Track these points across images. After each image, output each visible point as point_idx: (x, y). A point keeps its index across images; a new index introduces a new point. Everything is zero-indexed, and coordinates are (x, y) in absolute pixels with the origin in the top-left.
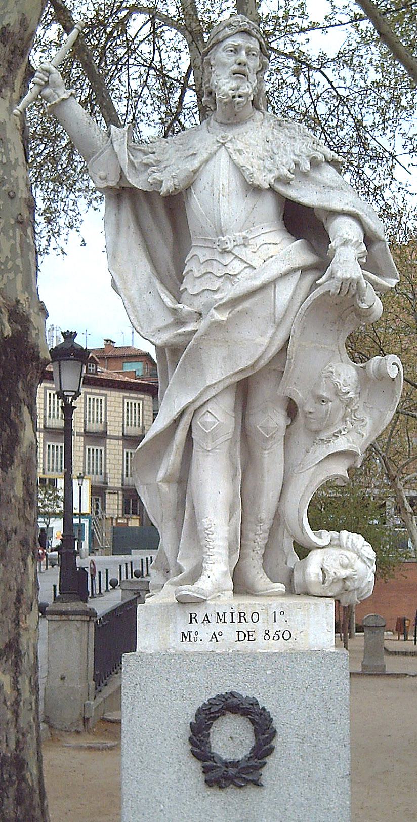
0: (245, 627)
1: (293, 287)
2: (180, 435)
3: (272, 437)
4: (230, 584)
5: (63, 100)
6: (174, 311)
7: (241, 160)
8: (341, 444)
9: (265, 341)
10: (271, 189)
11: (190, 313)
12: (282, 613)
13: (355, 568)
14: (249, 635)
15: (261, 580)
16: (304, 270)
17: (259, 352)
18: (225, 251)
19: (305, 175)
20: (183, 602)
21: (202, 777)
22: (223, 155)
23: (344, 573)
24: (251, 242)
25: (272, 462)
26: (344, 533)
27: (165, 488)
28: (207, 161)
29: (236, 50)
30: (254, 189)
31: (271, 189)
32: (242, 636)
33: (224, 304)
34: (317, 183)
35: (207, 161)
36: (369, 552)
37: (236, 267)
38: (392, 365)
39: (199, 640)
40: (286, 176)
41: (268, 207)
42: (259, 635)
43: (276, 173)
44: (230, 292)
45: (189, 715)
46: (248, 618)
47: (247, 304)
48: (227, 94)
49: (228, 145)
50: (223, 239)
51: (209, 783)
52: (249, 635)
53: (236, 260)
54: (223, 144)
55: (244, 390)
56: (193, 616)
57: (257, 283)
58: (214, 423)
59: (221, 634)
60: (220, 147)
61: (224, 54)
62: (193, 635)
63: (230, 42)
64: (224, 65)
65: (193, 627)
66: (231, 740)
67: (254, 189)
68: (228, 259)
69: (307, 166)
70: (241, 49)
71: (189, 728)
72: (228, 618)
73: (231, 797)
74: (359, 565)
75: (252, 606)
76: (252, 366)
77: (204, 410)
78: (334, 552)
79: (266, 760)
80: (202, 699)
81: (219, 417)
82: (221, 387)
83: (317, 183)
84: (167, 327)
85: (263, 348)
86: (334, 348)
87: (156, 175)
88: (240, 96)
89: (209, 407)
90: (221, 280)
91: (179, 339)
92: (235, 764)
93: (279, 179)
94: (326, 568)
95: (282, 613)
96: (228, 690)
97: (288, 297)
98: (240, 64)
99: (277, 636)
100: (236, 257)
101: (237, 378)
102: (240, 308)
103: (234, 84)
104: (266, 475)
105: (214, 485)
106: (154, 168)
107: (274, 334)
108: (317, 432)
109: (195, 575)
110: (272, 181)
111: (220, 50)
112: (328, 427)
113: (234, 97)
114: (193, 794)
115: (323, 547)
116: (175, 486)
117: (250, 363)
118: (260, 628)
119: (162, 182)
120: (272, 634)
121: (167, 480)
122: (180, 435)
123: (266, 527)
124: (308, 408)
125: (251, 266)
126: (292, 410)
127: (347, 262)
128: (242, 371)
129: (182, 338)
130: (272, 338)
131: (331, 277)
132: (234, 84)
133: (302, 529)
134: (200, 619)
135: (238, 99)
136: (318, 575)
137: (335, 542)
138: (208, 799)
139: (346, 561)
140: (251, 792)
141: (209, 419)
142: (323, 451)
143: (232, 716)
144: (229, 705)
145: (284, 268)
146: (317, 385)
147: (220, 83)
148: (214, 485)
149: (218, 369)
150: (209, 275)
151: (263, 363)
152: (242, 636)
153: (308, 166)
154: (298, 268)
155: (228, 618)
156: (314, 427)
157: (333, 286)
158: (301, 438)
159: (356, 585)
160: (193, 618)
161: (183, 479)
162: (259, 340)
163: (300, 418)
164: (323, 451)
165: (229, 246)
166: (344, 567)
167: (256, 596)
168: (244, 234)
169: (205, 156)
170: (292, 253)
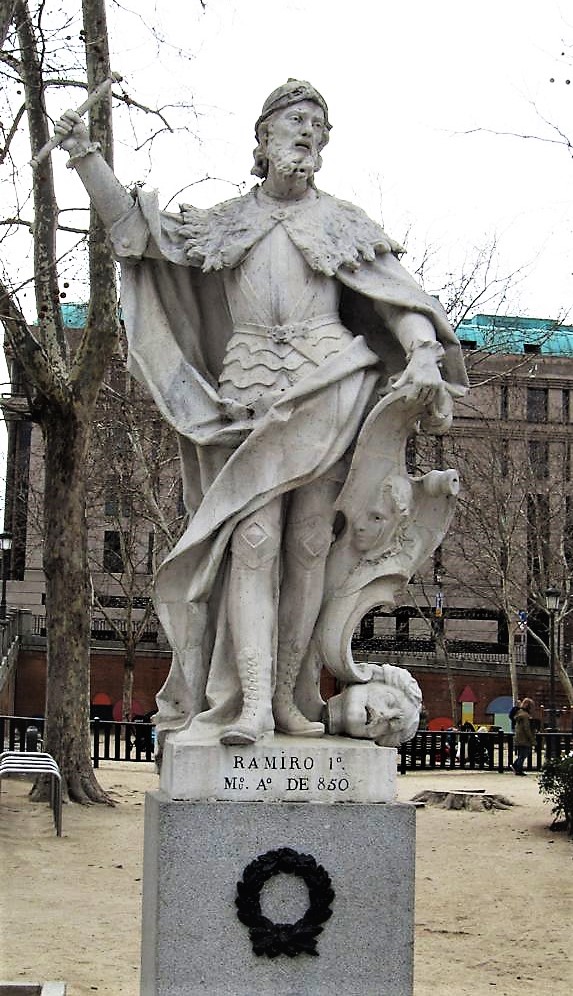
0: (296, 773)
1: (358, 389)
2: (218, 549)
3: (318, 556)
4: (272, 724)
5: (90, 153)
6: (221, 406)
7: (302, 241)
8: (390, 567)
9: (326, 446)
10: (335, 278)
11: (240, 410)
12: (339, 760)
13: (402, 707)
14: (301, 783)
15: (296, 719)
16: (367, 369)
17: (320, 459)
18: (282, 343)
19: (367, 263)
20: (228, 743)
21: (249, 945)
22: (279, 236)
23: (390, 713)
24: (311, 334)
25: (312, 581)
26: (387, 667)
27: (195, 609)
28: (261, 239)
29: (300, 119)
30: (316, 275)
31: (335, 278)
32: (293, 783)
33: (283, 404)
34: (379, 272)
35: (261, 239)
36: (416, 691)
37: (293, 361)
38: (447, 477)
39: (244, 787)
40: (351, 264)
41: (328, 297)
42: (313, 783)
43: (340, 260)
44: (292, 392)
45: (236, 873)
46: (301, 764)
47: (309, 405)
48: (288, 167)
49: (285, 223)
50: (281, 328)
51: (258, 952)
52: (301, 783)
53: (294, 354)
54: (280, 222)
55: (289, 502)
56: (294, 760)
57: (323, 381)
58: (262, 537)
59: (269, 781)
60: (276, 224)
61: (287, 122)
62: (238, 781)
63: (295, 108)
64: (286, 134)
65: (238, 773)
66: (284, 902)
67: (316, 275)
68: (285, 351)
69: (371, 255)
70: (306, 118)
71: (235, 889)
72: (278, 764)
73: (283, 966)
74: (405, 703)
75: (307, 750)
76: (309, 475)
77: (251, 522)
78: (380, 688)
79: (322, 925)
80: (252, 854)
81: (264, 532)
82: (272, 495)
83: (379, 272)
84: (209, 424)
85: (323, 454)
86: (395, 459)
87: (197, 249)
88: (302, 171)
89: (255, 519)
90: (277, 374)
91: (228, 438)
92: (287, 928)
93: (343, 266)
94: (372, 706)
95: (339, 760)
96: (281, 845)
97: (354, 398)
98: (304, 135)
99: (332, 786)
100: (294, 349)
101: (286, 489)
102: (301, 409)
103: (297, 156)
104: (306, 596)
105: (253, 609)
106: (192, 241)
107: (336, 440)
108: (364, 552)
109: (236, 708)
110: (337, 268)
111: (283, 116)
112: (377, 547)
113: (295, 170)
114: (239, 963)
115: (366, 683)
116: (204, 606)
117: (307, 471)
118: (314, 775)
119: (204, 257)
120: (327, 783)
121: (197, 600)
122: (218, 549)
123: (300, 657)
124: (360, 525)
125: (312, 362)
126: (340, 524)
127: (423, 369)
128: (298, 479)
129: (228, 438)
130: (333, 446)
131: (409, 381)
132: (297, 156)
133: (344, 662)
134: (246, 764)
135: (299, 173)
136: (362, 715)
137: (378, 677)
138: (256, 969)
139: (392, 700)
140: (305, 963)
141: (256, 531)
142: (367, 575)
143: (284, 875)
144: (283, 862)
145: (350, 366)
146: (373, 500)
147: (280, 154)
148: (253, 609)
149: (272, 478)
150: (261, 368)
151: (320, 472)
152: (293, 783)
153: (373, 256)
154: (363, 368)
155: (278, 764)
156: (363, 546)
157: (410, 393)
158: (345, 557)
159: (402, 726)
160: (238, 763)
161: (214, 600)
162: (318, 445)
163: (348, 537)
164: (367, 575)
165: (288, 337)
166: (391, 706)
167: (291, 736)
168: (303, 324)
169: (259, 234)
170: (354, 352)
